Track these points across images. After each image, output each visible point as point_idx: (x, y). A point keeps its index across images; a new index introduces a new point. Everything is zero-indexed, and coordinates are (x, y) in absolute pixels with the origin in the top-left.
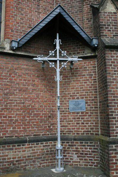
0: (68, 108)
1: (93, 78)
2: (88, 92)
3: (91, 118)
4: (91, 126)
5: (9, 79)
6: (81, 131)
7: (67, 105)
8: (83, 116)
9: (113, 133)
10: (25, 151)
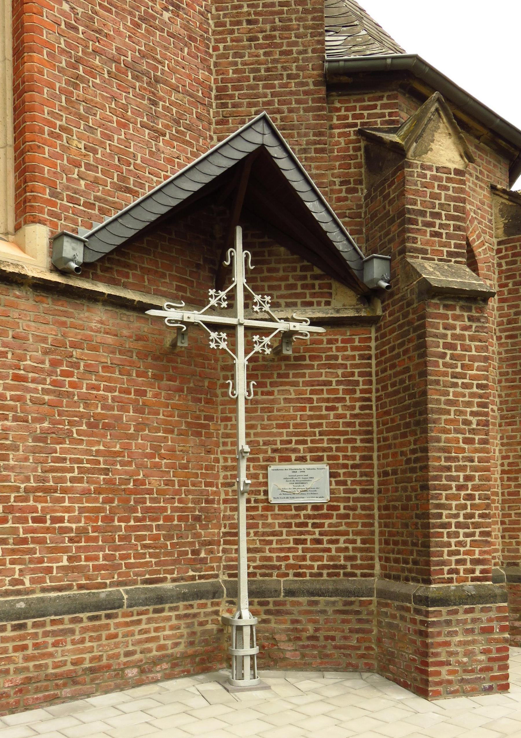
0: (266, 493)
1: (358, 395)
2: (338, 441)
3: (347, 524)
4: (346, 549)
5: (48, 381)
6: (311, 567)
7: (261, 480)
8: (320, 518)
9: (441, 572)
10: (116, 636)
